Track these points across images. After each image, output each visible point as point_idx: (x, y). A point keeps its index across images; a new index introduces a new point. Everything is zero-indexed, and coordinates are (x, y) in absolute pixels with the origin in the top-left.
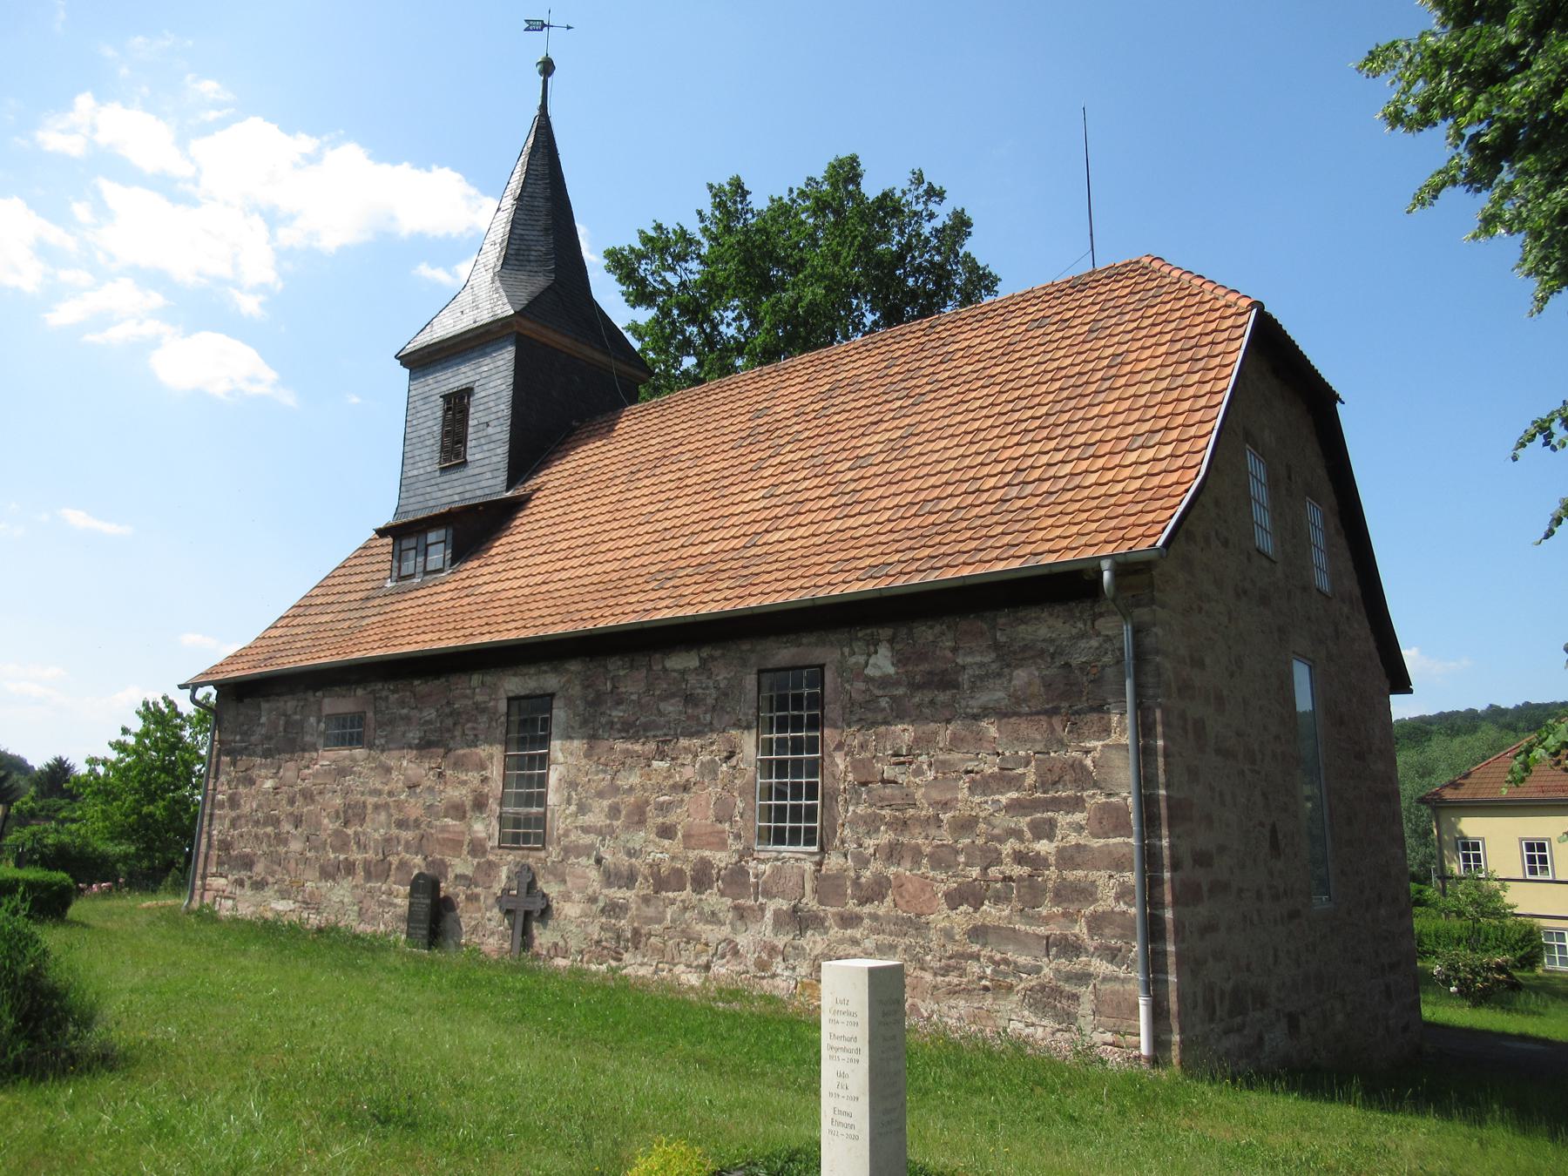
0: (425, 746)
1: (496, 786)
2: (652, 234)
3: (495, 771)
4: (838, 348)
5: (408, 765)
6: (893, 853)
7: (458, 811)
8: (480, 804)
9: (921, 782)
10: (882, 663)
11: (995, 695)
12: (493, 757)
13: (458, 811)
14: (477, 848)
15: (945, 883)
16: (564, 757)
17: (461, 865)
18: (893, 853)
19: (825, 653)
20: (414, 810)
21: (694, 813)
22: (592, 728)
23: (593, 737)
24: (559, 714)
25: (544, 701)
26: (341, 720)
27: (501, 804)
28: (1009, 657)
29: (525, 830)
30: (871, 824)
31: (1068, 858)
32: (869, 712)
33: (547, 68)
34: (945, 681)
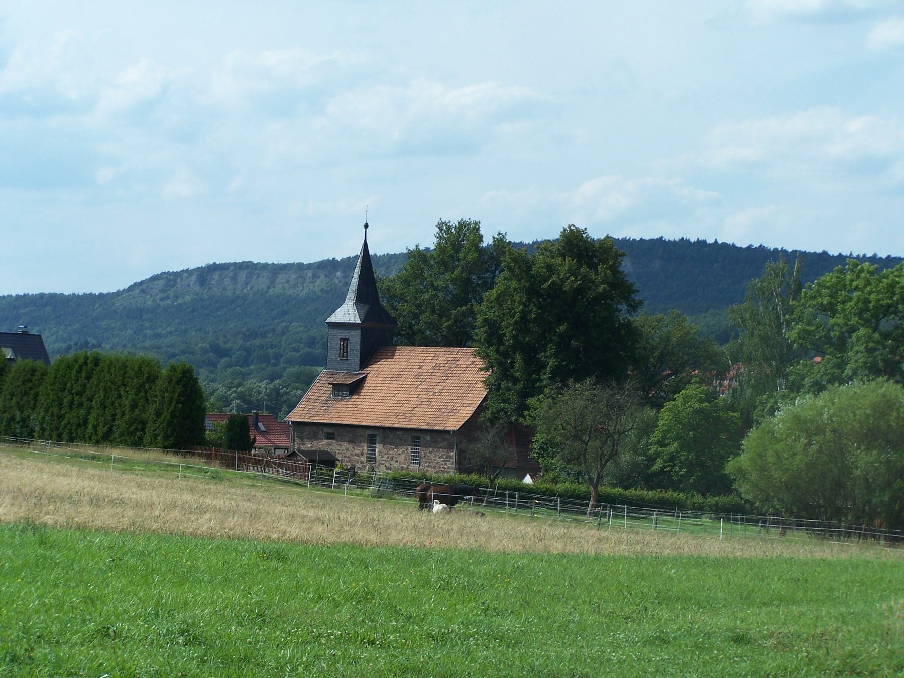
0: (350, 442)
1: (366, 451)
2: (496, 236)
3: (365, 448)
4: (127, 476)
5: (345, 445)
6: (428, 466)
7: (358, 455)
8: (362, 454)
9: (432, 456)
10: (428, 438)
11: (441, 445)
12: (365, 447)
13: (358, 455)
14: (362, 462)
15: (434, 471)
16: (378, 448)
17: (358, 465)
18: (428, 466)
19: (421, 436)
20: (348, 454)
21: (401, 458)
22: (384, 443)
23: (384, 444)
24: (378, 439)
25: (375, 436)
26: (329, 434)
27: (585, 514)
28: (444, 440)
29: (371, 459)
30: (426, 462)
31: (449, 468)
32: (426, 446)
33: (366, 226)
34: (436, 442)
